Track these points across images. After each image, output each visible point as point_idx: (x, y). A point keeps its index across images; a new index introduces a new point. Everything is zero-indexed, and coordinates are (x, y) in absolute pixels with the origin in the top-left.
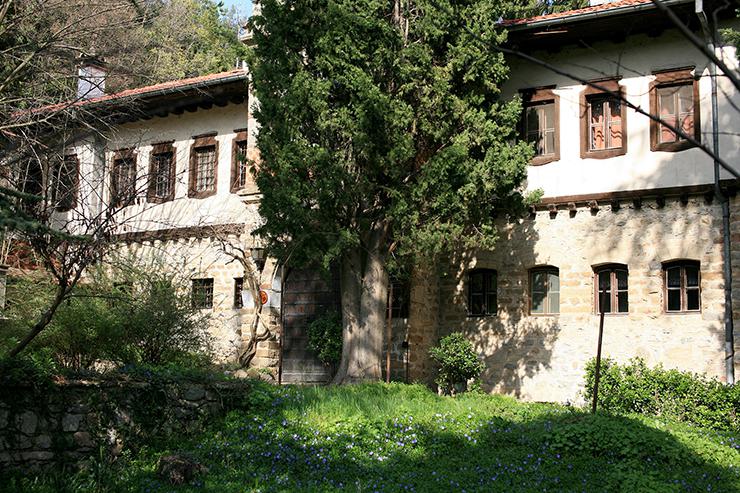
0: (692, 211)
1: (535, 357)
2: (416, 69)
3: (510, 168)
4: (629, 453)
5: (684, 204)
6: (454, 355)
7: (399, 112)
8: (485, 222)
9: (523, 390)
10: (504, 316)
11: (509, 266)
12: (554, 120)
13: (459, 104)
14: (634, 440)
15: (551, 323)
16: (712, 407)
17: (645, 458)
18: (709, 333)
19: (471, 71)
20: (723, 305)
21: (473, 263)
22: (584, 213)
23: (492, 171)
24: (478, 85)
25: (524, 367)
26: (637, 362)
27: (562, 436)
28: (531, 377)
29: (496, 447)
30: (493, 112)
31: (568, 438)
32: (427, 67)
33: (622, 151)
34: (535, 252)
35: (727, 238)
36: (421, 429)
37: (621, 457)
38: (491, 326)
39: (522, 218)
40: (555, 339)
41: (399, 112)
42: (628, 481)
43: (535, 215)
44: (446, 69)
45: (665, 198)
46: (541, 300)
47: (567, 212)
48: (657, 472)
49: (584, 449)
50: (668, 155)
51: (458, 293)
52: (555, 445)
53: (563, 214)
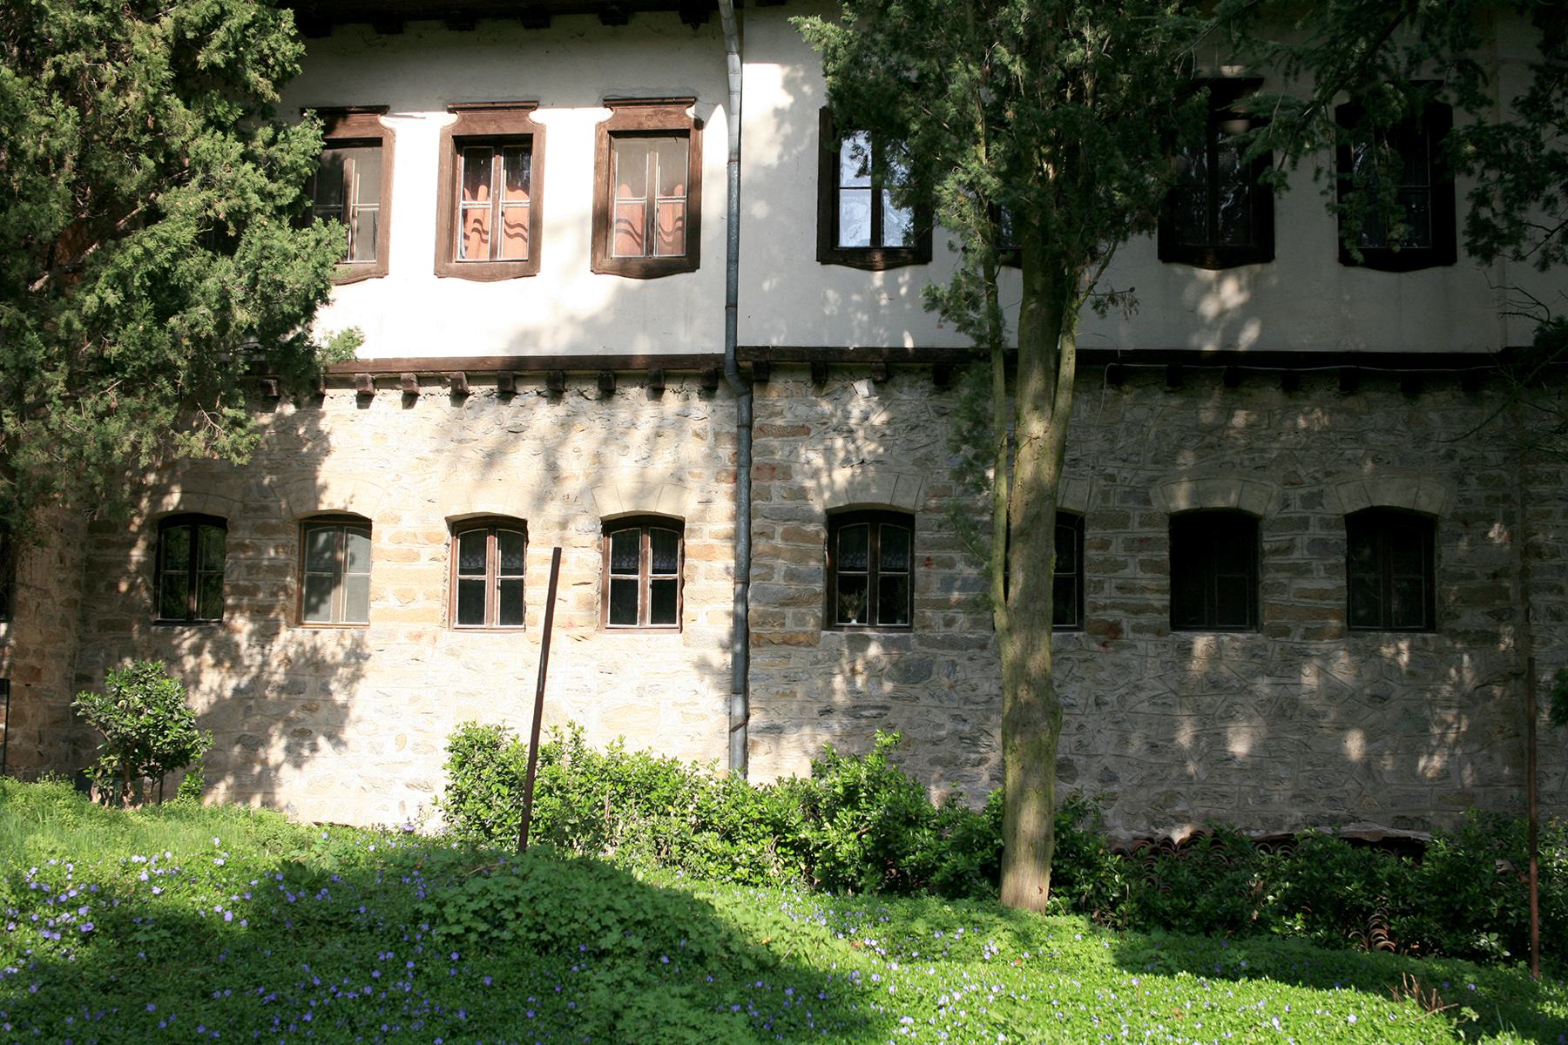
0: (672, 401)
1: (309, 721)
2: (90, 19)
3: (296, 277)
4: (619, 944)
5: (657, 393)
6: (139, 712)
7: (37, 119)
8: (229, 401)
9: (282, 795)
10: (243, 627)
11: (257, 508)
12: (380, 186)
13: (182, 117)
14: (625, 915)
15: (348, 642)
16: (728, 836)
17: (654, 956)
18: (695, 674)
19: (215, 43)
20: (729, 614)
21: (173, 500)
22: (435, 400)
23: (254, 280)
24: (229, 78)
25: (283, 742)
26: (568, 735)
27: (460, 909)
28: (298, 765)
29: (298, 935)
30: (257, 145)
31: (475, 912)
32: (114, 18)
33: (529, 266)
34: (320, 481)
35: (744, 471)
36: (100, 894)
37: (601, 955)
38: (208, 645)
39: (297, 404)
40: (356, 677)
41: (37, 119)
42: (635, 1013)
43: (323, 396)
44: (156, 29)
45: (616, 377)
46: (329, 593)
47: (395, 396)
48: (688, 989)
49: (516, 939)
50: (614, 281)
51: (133, 568)
52: (444, 929)
53: (388, 400)
